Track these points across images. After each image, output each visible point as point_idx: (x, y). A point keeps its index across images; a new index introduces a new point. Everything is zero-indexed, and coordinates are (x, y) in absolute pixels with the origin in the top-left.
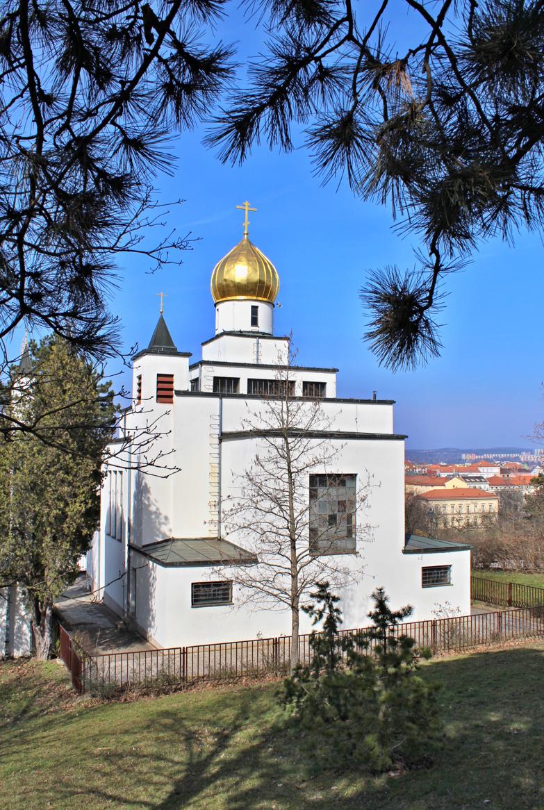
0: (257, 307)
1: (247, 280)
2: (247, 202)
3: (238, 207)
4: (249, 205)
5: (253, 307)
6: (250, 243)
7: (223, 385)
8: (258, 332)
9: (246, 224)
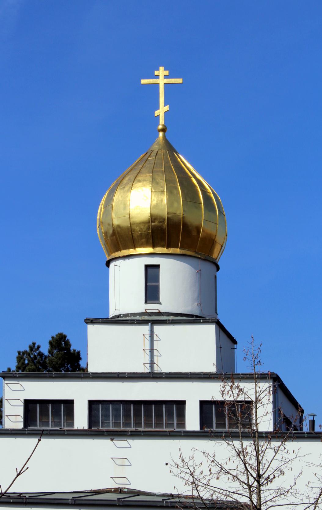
0: (157, 266)
1: (152, 215)
2: (161, 69)
3: (143, 81)
4: (167, 73)
5: (147, 267)
6: (169, 147)
7: (44, 413)
8: (159, 314)
9: (162, 110)
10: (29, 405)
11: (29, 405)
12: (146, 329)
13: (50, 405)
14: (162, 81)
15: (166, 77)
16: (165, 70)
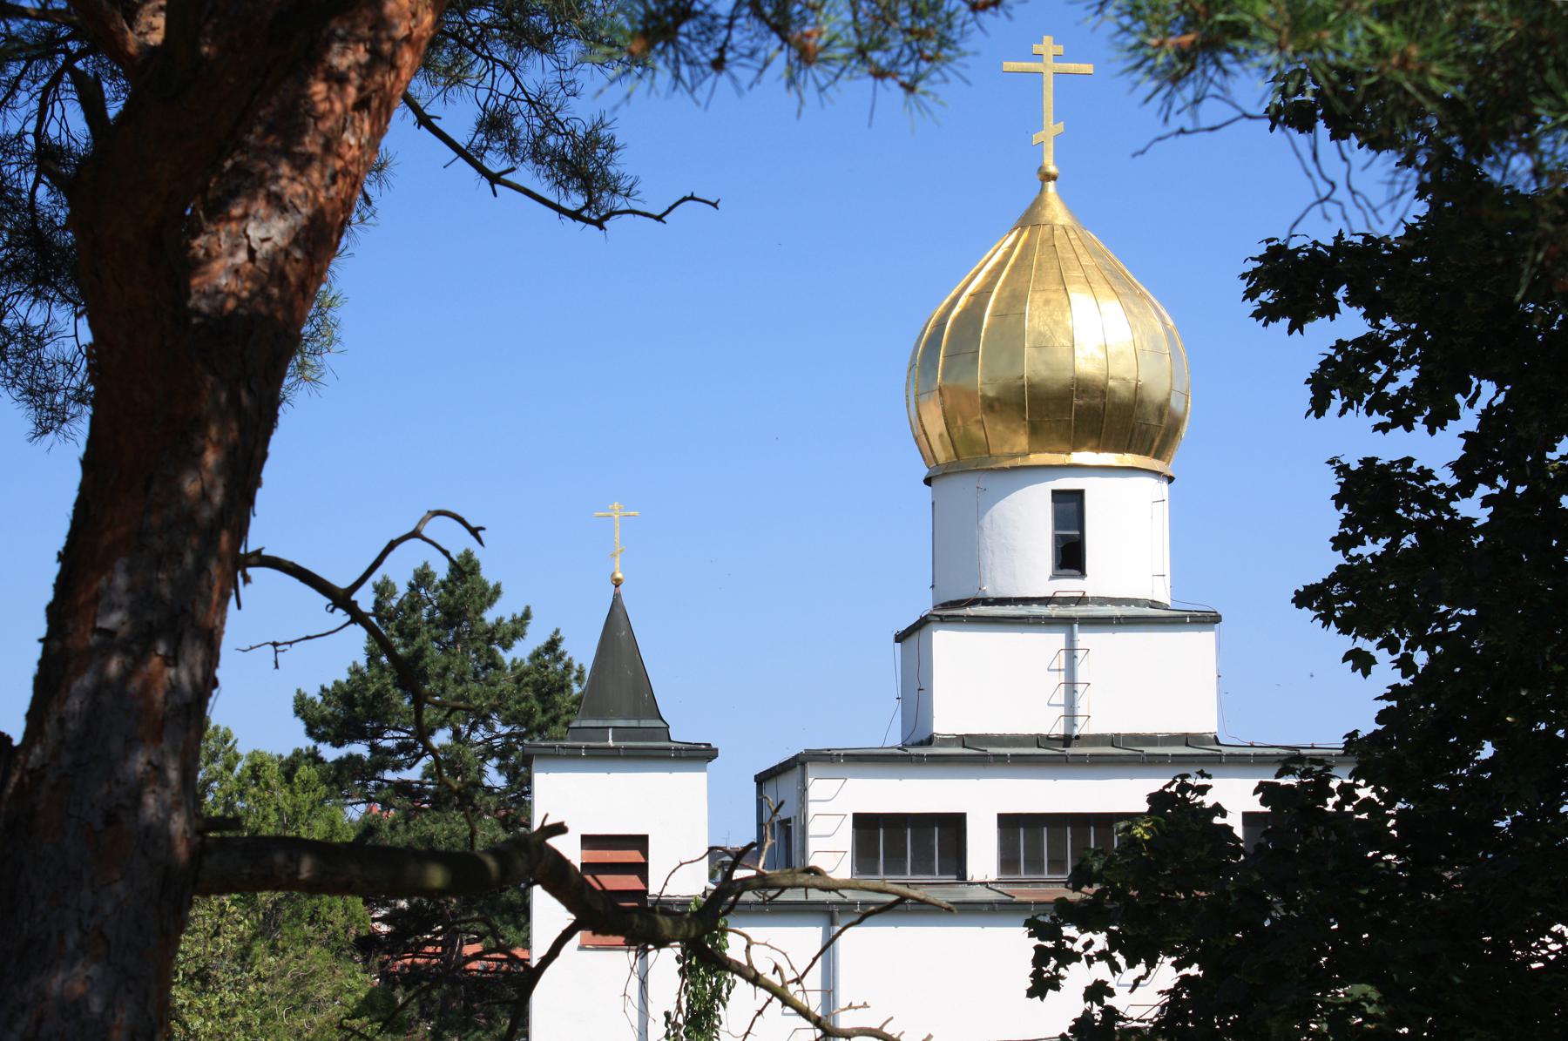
0: (1078, 495)
1: (1137, 389)
2: (1048, 39)
4: (1060, 49)
5: (1057, 494)
8: (1081, 600)
10: (865, 824)
11: (865, 824)
12: (1057, 639)
13: (1045, 829)
14: (1049, 68)
15: (1057, 58)
16: (1055, 43)
